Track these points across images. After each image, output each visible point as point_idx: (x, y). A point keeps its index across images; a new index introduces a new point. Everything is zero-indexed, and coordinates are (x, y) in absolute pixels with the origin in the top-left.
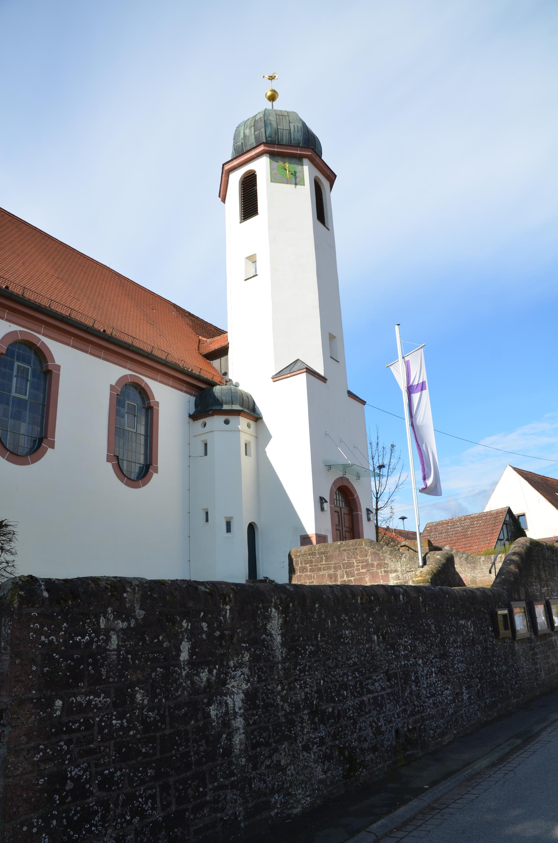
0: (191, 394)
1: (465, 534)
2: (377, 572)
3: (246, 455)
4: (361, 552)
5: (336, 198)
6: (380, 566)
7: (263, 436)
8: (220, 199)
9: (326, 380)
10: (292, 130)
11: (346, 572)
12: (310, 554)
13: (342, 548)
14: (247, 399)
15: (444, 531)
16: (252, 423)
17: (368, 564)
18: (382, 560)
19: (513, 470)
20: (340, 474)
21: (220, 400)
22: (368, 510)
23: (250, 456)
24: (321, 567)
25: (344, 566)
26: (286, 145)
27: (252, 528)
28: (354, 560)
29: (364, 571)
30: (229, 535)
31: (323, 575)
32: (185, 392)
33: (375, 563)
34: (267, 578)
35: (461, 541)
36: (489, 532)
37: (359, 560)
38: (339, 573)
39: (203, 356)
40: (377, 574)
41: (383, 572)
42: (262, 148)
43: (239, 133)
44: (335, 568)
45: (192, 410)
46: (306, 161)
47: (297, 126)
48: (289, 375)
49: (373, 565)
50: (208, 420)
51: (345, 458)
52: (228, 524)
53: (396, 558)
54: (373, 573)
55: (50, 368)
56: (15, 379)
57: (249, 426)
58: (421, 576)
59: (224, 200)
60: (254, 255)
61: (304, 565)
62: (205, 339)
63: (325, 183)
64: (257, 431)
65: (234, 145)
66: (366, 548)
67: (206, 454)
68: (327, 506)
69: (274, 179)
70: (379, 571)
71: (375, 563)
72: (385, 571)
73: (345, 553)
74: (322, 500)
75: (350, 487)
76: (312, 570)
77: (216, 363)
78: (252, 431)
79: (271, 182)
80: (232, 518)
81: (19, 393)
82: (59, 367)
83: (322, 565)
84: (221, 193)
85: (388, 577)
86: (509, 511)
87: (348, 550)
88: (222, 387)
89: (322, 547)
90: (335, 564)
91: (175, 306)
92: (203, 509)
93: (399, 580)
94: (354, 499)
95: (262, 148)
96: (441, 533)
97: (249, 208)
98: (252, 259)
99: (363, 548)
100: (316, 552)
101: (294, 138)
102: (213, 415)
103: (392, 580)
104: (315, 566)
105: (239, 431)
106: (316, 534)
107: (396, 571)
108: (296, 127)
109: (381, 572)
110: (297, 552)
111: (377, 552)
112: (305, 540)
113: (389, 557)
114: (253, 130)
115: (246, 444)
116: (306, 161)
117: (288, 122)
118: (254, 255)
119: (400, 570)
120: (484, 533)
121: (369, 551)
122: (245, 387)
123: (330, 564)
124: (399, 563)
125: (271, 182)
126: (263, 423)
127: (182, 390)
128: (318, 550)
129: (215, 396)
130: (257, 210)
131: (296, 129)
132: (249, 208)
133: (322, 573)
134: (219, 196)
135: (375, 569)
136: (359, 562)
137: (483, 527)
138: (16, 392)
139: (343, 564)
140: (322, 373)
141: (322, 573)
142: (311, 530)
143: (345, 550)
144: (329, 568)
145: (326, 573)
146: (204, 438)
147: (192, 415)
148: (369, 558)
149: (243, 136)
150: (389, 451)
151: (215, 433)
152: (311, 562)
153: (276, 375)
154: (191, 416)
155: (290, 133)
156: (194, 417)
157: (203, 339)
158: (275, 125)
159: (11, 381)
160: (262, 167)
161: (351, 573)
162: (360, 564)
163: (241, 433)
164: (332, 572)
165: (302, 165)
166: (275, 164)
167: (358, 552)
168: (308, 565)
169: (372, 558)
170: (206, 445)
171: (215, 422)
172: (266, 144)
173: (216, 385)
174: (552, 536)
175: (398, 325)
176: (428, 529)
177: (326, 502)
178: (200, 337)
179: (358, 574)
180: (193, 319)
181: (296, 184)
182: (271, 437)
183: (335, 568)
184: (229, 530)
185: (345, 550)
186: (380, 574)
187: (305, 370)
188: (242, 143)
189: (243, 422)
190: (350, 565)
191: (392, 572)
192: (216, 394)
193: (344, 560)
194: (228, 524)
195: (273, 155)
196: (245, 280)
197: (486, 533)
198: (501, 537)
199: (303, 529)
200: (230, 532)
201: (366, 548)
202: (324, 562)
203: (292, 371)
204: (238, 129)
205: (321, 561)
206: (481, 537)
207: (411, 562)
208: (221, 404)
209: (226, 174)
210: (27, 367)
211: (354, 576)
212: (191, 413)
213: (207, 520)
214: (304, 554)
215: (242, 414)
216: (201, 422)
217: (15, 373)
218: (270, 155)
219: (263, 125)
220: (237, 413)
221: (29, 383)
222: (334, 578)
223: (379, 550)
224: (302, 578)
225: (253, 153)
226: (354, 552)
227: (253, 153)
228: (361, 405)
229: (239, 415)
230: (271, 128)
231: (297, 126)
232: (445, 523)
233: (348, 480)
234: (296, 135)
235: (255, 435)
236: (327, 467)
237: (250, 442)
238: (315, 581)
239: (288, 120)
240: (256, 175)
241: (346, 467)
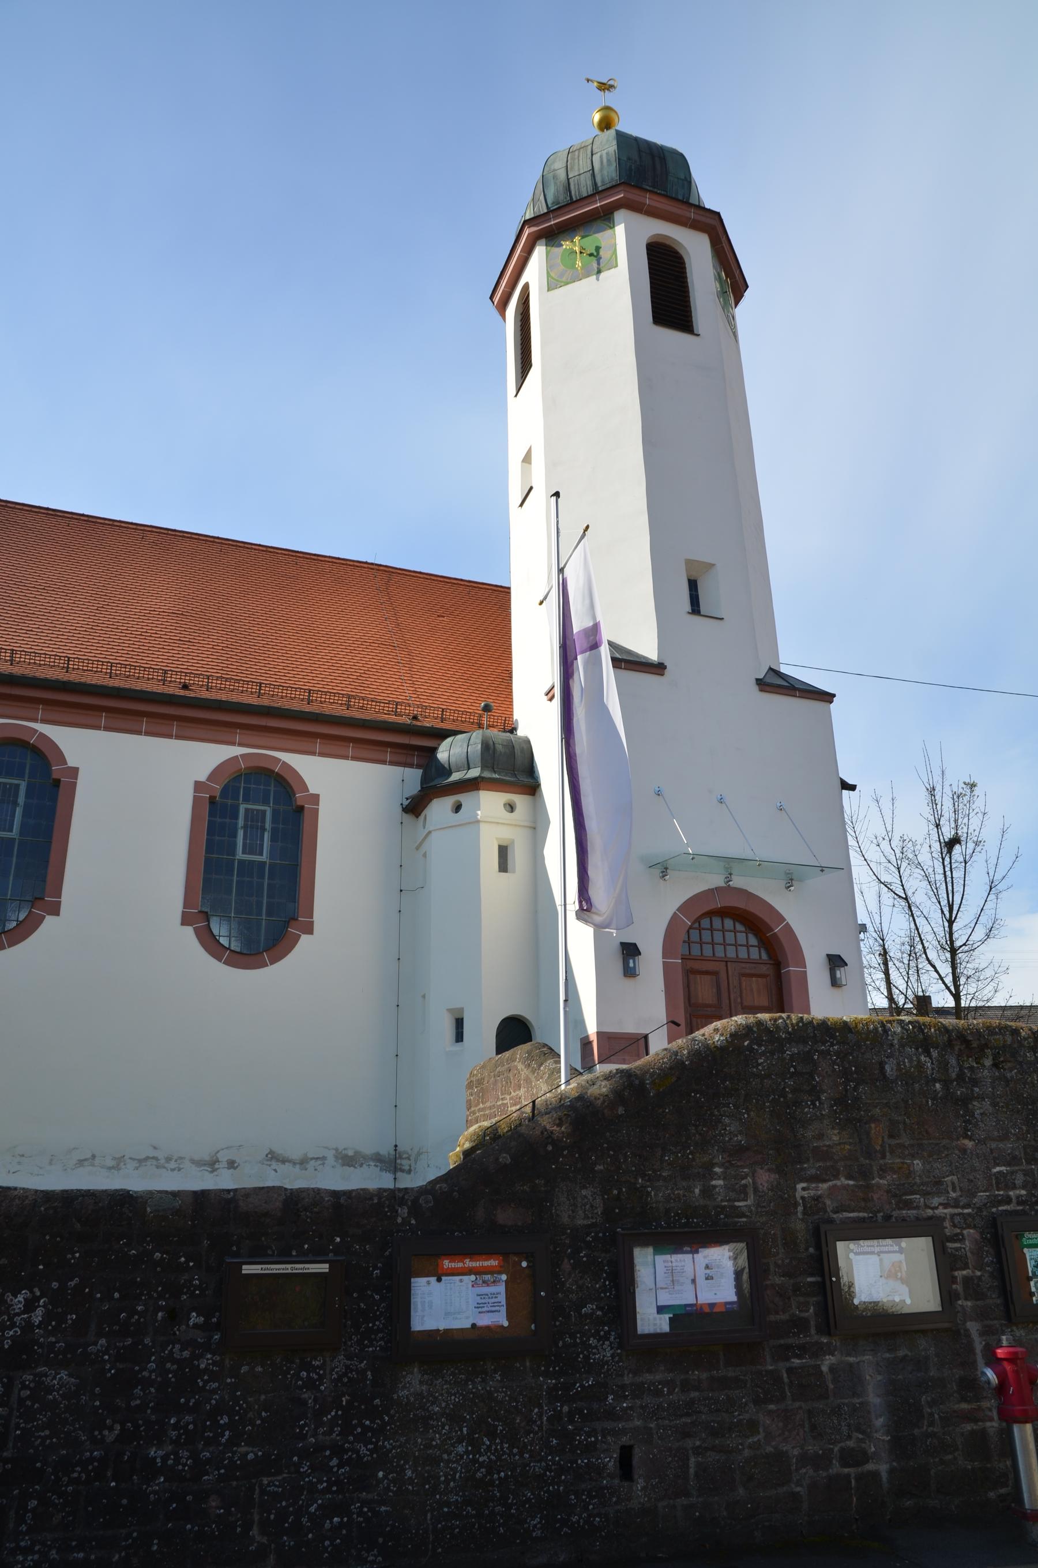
21: (446, 766)
30: (458, 1047)
32: (392, 763)
52: (459, 1023)
55: (299, 803)
56: (241, 834)
57: (511, 807)
80: (462, 1010)
81: (250, 854)
82: (316, 798)
95: (527, 231)
101: (603, 181)
105: (478, 822)
108: (604, 156)
126: (541, 796)
127: (383, 762)
138: (243, 853)
151: (433, 834)
155: (593, 175)
159: (234, 835)
163: (482, 826)
181: (599, 272)
189: (489, 804)
208: (449, 773)
210: (263, 808)
215: (481, 785)
217: (241, 822)
221: (266, 835)
229: (478, 789)
231: (607, 154)
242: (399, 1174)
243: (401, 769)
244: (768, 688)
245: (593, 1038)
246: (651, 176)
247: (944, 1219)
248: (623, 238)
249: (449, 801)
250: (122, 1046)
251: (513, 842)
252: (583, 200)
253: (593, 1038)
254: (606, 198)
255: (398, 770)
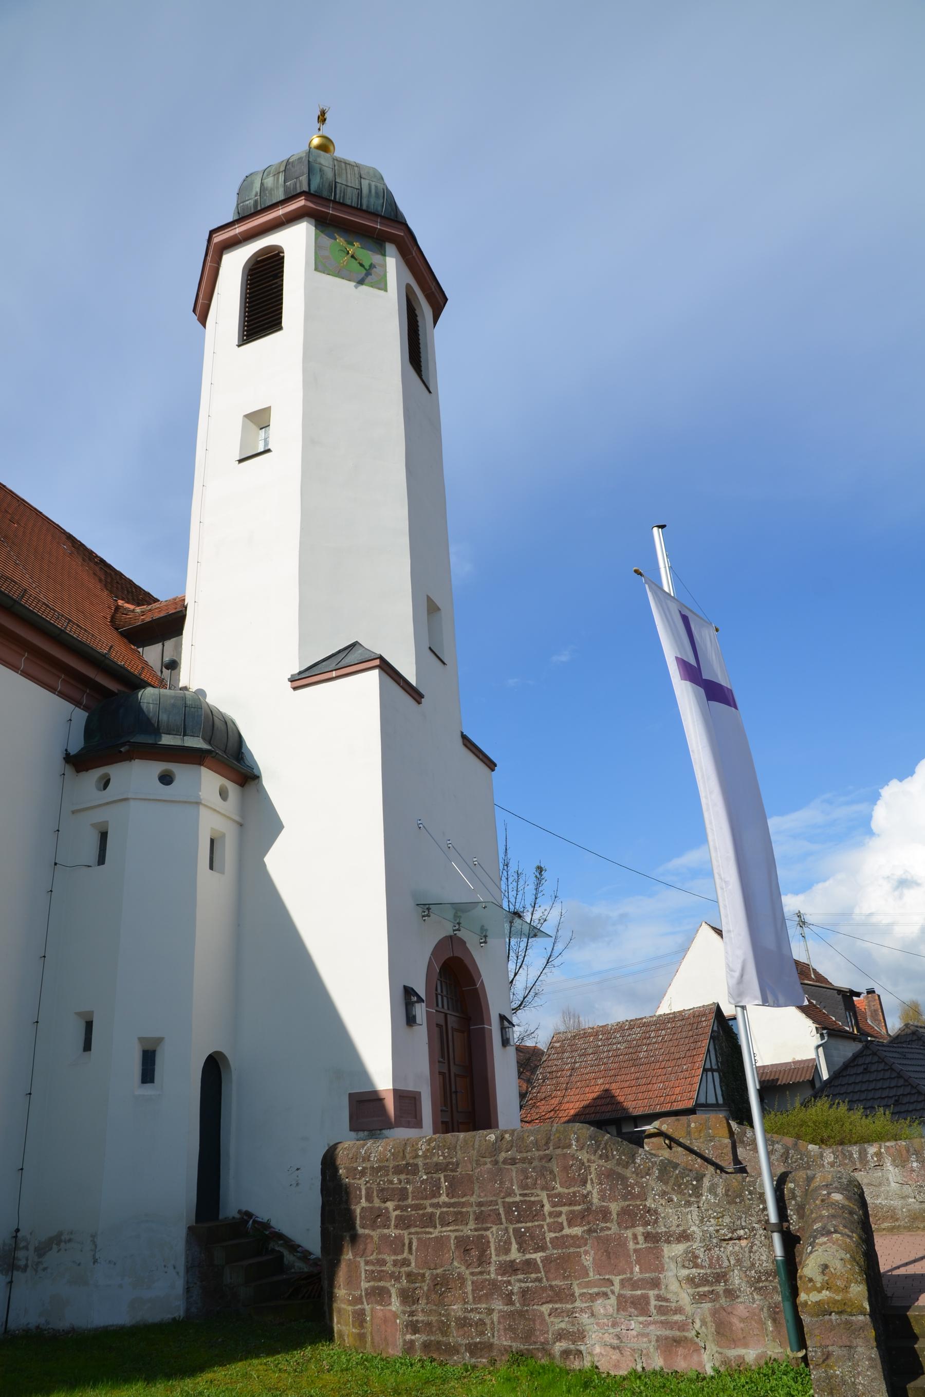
0: (77, 703)
1: (634, 1056)
3: (211, 868)
4: (566, 1169)
5: (442, 338)
6: (629, 1217)
7: (258, 822)
8: (195, 318)
9: (422, 696)
11: (516, 1231)
12: (398, 1170)
14: (223, 727)
15: (590, 1051)
16: (232, 788)
17: (588, 1209)
18: (635, 1197)
20: (447, 929)
21: (154, 721)
22: (503, 1018)
23: (222, 872)
24: (432, 1215)
25: (508, 1211)
26: (350, 207)
27: (214, 1070)
28: (544, 1197)
29: (577, 1231)
30: (147, 1090)
31: (441, 1242)
33: (614, 1207)
37: (559, 1195)
39: (122, 634)
40: (622, 1243)
41: (641, 1239)
42: (301, 203)
44: (479, 1218)
45: (76, 745)
46: (390, 248)
47: (376, 187)
48: (334, 674)
49: (605, 1214)
52: (149, 1060)
53: (681, 1192)
54: (607, 1239)
57: (223, 794)
59: (203, 319)
60: (266, 411)
61: (377, 1203)
62: (131, 607)
65: (238, 205)
66: (583, 1156)
67: (101, 860)
68: (420, 1011)
69: (322, 264)
70: (629, 1233)
71: (614, 1207)
72: (647, 1236)
73: (513, 1172)
74: (409, 992)
75: (467, 962)
78: (231, 806)
79: (316, 269)
80: (160, 1040)
83: (437, 1206)
84: (200, 301)
85: (659, 1256)
86: (719, 1011)
87: (523, 1160)
89: (438, 1147)
90: (480, 1204)
91: (70, 537)
92: (79, 1014)
93: (696, 1266)
95: (301, 203)
96: (584, 1055)
97: (262, 312)
98: (259, 419)
99: (573, 1157)
100: (420, 1162)
102: (129, 757)
103: (673, 1266)
104: (416, 1207)
106: (395, 1091)
107: (684, 1237)
109: (635, 1237)
110: (355, 1158)
111: (620, 1170)
112: (366, 1110)
113: (658, 1187)
114: (281, 177)
115: (212, 841)
116: (390, 248)
117: (357, 176)
118: (266, 411)
119: (699, 1235)
120: (672, 1057)
121: (593, 1167)
122: (219, 699)
124: (694, 1208)
125: (316, 269)
128: (425, 1156)
130: (281, 323)
131: (373, 191)
132: (262, 312)
133: (436, 1233)
134: (194, 311)
136: (559, 1200)
137: (671, 1044)
139: (508, 1207)
140: (413, 680)
141: (436, 1233)
142: (383, 1079)
143: (513, 1161)
144: (460, 1219)
145: (450, 1232)
146: (99, 816)
147: (75, 756)
148: (594, 1191)
149: (258, 190)
150: (532, 881)
151: (132, 803)
152: (403, 1194)
153: (300, 673)
154: (69, 759)
156: (78, 762)
157: (127, 605)
158: (329, 174)
160: (296, 242)
161: (532, 1237)
162: (564, 1209)
163: (203, 811)
164: (468, 1229)
166: (326, 240)
167: (556, 1170)
168: (390, 1205)
170: (104, 836)
171: (136, 777)
172: (307, 194)
173: (144, 687)
174: (789, 1060)
176: (558, 1045)
177: (420, 1000)
178: (120, 602)
184: (148, 1075)
185: (513, 1161)
186: (631, 1246)
187: (377, 662)
188: (256, 201)
189: (209, 782)
190: (531, 1211)
192: (144, 706)
193: (510, 1193)
194: (149, 1060)
196: (240, 461)
197: (677, 1056)
198: (708, 1066)
199: (362, 1073)
200: (152, 1081)
201: (583, 1156)
202: (444, 1198)
203: (343, 664)
204: (249, 179)
205: (435, 1194)
206: (669, 1064)
207: (733, 1209)
211: (543, 1248)
212: (73, 751)
213: (87, 1046)
214: (380, 1169)
216: (96, 774)
218: (316, 220)
219: (306, 170)
220: (194, 757)
222: (475, 1253)
223: (626, 1166)
224: (370, 1247)
225: (280, 212)
227: (280, 212)
229: (200, 763)
230: (321, 177)
231: (376, 187)
232: (590, 1035)
233: (464, 943)
234: (372, 200)
235: (237, 818)
237: (223, 836)
238: (412, 1259)
239: (357, 172)
240: (283, 258)
241: (460, 910)
242: (15, 1273)
243: (72, 707)
244: (469, 745)
245: (846, 1203)
248: (367, 267)
249: (158, 767)
250: (30, 1303)
251: (224, 836)
252: (342, 205)
253: (846, 1203)
255: (67, 706)
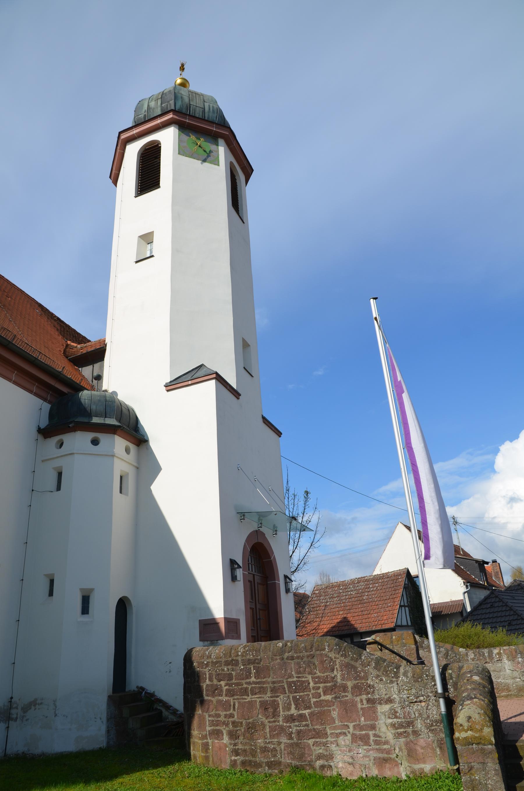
0: (45, 400)
1: (361, 599)
2: (353, 700)
3: (121, 492)
4: (322, 662)
6: (358, 689)
7: (148, 467)
9: (240, 395)
10: (207, 109)
11: (294, 698)
12: (227, 663)
13: (287, 654)
14: (127, 413)
15: (336, 595)
16: (132, 446)
17: (335, 685)
18: (361, 678)
19: (404, 528)
21: (88, 409)
22: (286, 577)
24: (246, 689)
25: (290, 687)
27: (123, 606)
28: (310, 678)
29: (329, 697)
30: (85, 618)
31: (251, 704)
33: (350, 684)
34: (143, 689)
35: (356, 607)
36: (388, 597)
37: (318, 677)
38: (281, 699)
39: (70, 360)
40: (354, 704)
41: (365, 702)
42: (170, 116)
43: (143, 105)
44: (273, 690)
45: (44, 423)
46: (221, 141)
47: (213, 107)
48: (190, 382)
49: (344, 688)
50: (68, 438)
51: (262, 502)
53: (387, 676)
54: (346, 702)
57: (127, 451)
58: (471, 729)
59: (115, 182)
60: (151, 234)
61: (215, 682)
62: (75, 345)
63: (241, 176)
64: (139, 459)
66: (332, 655)
67: (59, 488)
69: (182, 151)
70: (358, 699)
71: (350, 684)
72: (369, 701)
73: (292, 664)
74: (233, 562)
75: (266, 545)
76: (230, 693)
77: (87, 371)
78: (131, 457)
79: (179, 153)
80: (92, 590)
83: (249, 683)
84: (114, 172)
86: (408, 572)
87: (298, 657)
88: (93, 392)
89: (249, 650)
90: (274, 683)
91: (40, 305)
93: (396, 717)
94: (271, 561)
95: (170, 116)
96: (332, 598)
97: (148, 178)
98: (147, 238)
99: (326, 655)
100: (239, 659)
102: (74, 430)
103: (383, 717)
104: (237, 684)
106: (226, 619)
107: (390, 701)
109: (361, 701)
110: (203, 657)
111: (353, 663)
112: (208, 629)
113: (375, 672)
114: (159, 102)
115: (121, 477)
116: (221, 141)
117: (202, 101)
118: (151, 234)
119: (397, 699)
120: (382, 599)
121: (338, 661)
122: (127, 395)
123: (264, 683)
124: (395, 684)
125: (179, 153)
128: (242, 655)
129: (80, 403)
132: (148, 178)
134: (110, 177)
135: (350, 696)
136: (318, 680)
137: (381, 591)
139: (289, 684)
141: (248, 699)
142: (218, 612)
143: (292, 658)
144: (263, 691)
145: (257, 698)
146: (57, 463)
148: (338, 674)
149: (146, 109)
150: (302, 499)
151: (76, 456)
152: (230, 677)
153: (171, 382)
154: (40, 431)
156: (45, 433)
157: (73, 344)
158: (186, 100)
160: (168, 138)
161: (303, 701)
162: (321, 685)
163: (116, 459)
164: (267, 697)
165: (218, 145)
166: (185, 137)
167: (317, 663)
168: (223, 683)
169: (343, 675)
170: (60, 474)
171: (78, 441)
172: (174, 111)
174: (448, 600)
175: (375, 298)
176: (317, 592)
178: (69, 342)
179: (318, 704)
180: (62, 325)
182: (161, 469)
183: (274, 690)
184: (85, 610)
185: (292, 658)
186: (359, 706)
187: (214, 376)
188: (145, 115)
189: (119, 444)
190: (302, 686)
191: (381, 701)
192: (83, 401)
193: (291, 676)
195: (183, 127)
196: (137, 262)
197: (385, 598)
200: (87, 613)
201: (332, 655)
202: (253, 679)
203: (195, 376)
204: (141, 103)
205: (248, 677)
206: (380, 603)
207: (417, 685)
209: (122, 145)
211: (309, 708)
212: (42, 426)
213: (51, 594)
214: (217, 662)
216: (55, 439)
218: (179, 126)
219: (173, 98)
220: (111, 430)
222: (271, 710)
223: (356, 661)
224: (211, 707)
225: (159, 121)
226: (310, 662)
227: (159, 121)
228: (276, 436)
229: (115, 433)
231: (213, 107)
232: (336, 586)
234: (211, 115)
235: (135, 464)
236: (239, 516)
238: (235, 713)
239: (202, 99)
241: (261, 516)
245: (481, 681)
246: (203, 126)
247: (247, 722)
249: (90, 436)
253: (481, 681)
254: (219, 129)
